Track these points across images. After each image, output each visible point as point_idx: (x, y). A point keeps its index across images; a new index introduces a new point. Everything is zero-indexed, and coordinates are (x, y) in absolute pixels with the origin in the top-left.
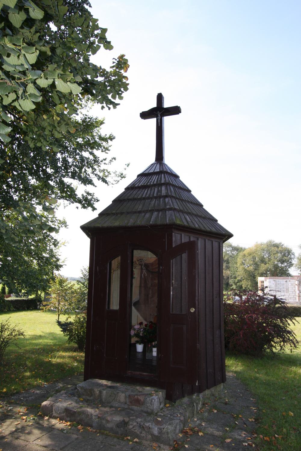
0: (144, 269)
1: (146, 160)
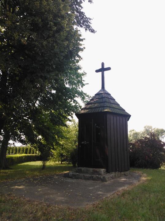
1: (98, 89)
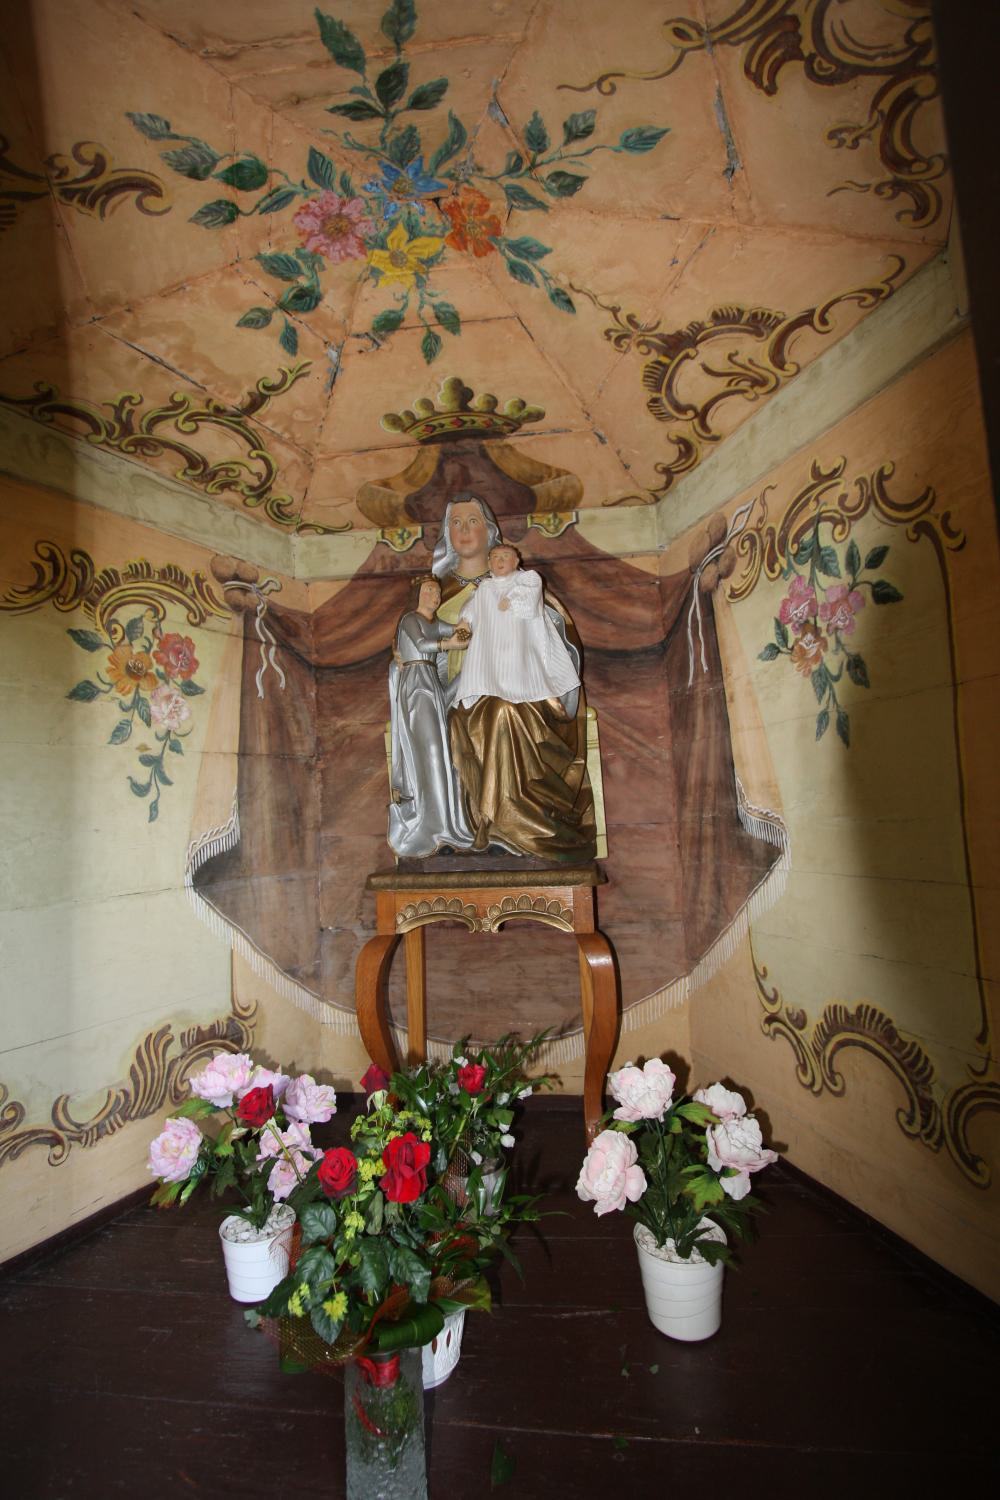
0: (269, 644)
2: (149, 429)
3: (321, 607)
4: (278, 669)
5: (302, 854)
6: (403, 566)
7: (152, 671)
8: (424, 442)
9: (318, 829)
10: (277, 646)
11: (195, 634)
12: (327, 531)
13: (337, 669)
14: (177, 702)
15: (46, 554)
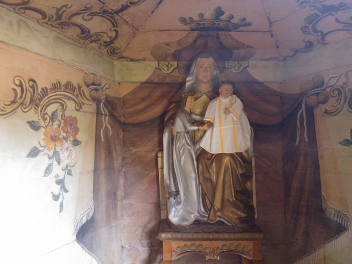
0: (106, 115)
2: (69, 18)
3: (126, 95)
4: (109, 127)
5: (116, 213)
6: (168, 80)
7: (61, 136)
8: (193, 30)
9: (122, 200)
10: (109, 115)
11: (78, 115)
12: (132, 60)
13: (134, 125)
14: (71, 150)
15: (18, 83)
